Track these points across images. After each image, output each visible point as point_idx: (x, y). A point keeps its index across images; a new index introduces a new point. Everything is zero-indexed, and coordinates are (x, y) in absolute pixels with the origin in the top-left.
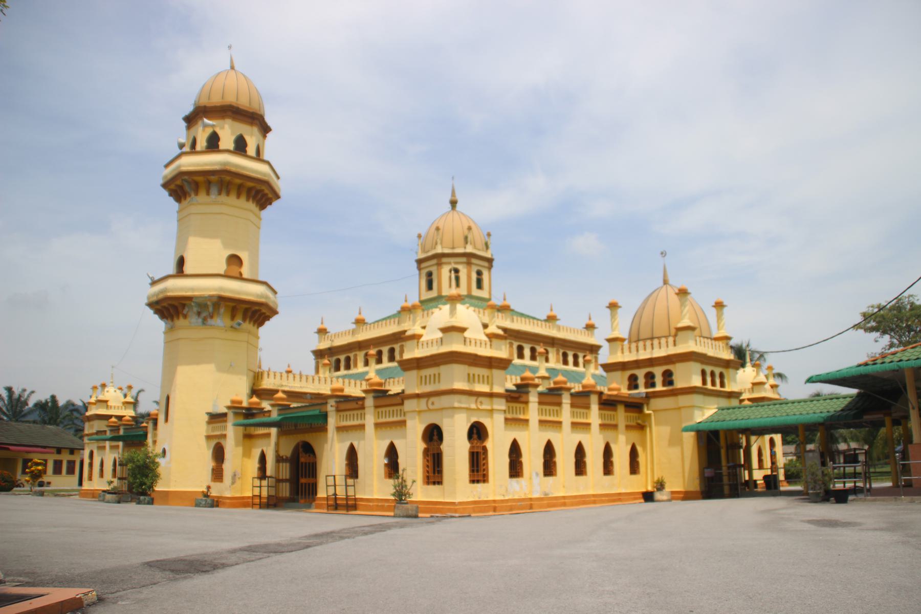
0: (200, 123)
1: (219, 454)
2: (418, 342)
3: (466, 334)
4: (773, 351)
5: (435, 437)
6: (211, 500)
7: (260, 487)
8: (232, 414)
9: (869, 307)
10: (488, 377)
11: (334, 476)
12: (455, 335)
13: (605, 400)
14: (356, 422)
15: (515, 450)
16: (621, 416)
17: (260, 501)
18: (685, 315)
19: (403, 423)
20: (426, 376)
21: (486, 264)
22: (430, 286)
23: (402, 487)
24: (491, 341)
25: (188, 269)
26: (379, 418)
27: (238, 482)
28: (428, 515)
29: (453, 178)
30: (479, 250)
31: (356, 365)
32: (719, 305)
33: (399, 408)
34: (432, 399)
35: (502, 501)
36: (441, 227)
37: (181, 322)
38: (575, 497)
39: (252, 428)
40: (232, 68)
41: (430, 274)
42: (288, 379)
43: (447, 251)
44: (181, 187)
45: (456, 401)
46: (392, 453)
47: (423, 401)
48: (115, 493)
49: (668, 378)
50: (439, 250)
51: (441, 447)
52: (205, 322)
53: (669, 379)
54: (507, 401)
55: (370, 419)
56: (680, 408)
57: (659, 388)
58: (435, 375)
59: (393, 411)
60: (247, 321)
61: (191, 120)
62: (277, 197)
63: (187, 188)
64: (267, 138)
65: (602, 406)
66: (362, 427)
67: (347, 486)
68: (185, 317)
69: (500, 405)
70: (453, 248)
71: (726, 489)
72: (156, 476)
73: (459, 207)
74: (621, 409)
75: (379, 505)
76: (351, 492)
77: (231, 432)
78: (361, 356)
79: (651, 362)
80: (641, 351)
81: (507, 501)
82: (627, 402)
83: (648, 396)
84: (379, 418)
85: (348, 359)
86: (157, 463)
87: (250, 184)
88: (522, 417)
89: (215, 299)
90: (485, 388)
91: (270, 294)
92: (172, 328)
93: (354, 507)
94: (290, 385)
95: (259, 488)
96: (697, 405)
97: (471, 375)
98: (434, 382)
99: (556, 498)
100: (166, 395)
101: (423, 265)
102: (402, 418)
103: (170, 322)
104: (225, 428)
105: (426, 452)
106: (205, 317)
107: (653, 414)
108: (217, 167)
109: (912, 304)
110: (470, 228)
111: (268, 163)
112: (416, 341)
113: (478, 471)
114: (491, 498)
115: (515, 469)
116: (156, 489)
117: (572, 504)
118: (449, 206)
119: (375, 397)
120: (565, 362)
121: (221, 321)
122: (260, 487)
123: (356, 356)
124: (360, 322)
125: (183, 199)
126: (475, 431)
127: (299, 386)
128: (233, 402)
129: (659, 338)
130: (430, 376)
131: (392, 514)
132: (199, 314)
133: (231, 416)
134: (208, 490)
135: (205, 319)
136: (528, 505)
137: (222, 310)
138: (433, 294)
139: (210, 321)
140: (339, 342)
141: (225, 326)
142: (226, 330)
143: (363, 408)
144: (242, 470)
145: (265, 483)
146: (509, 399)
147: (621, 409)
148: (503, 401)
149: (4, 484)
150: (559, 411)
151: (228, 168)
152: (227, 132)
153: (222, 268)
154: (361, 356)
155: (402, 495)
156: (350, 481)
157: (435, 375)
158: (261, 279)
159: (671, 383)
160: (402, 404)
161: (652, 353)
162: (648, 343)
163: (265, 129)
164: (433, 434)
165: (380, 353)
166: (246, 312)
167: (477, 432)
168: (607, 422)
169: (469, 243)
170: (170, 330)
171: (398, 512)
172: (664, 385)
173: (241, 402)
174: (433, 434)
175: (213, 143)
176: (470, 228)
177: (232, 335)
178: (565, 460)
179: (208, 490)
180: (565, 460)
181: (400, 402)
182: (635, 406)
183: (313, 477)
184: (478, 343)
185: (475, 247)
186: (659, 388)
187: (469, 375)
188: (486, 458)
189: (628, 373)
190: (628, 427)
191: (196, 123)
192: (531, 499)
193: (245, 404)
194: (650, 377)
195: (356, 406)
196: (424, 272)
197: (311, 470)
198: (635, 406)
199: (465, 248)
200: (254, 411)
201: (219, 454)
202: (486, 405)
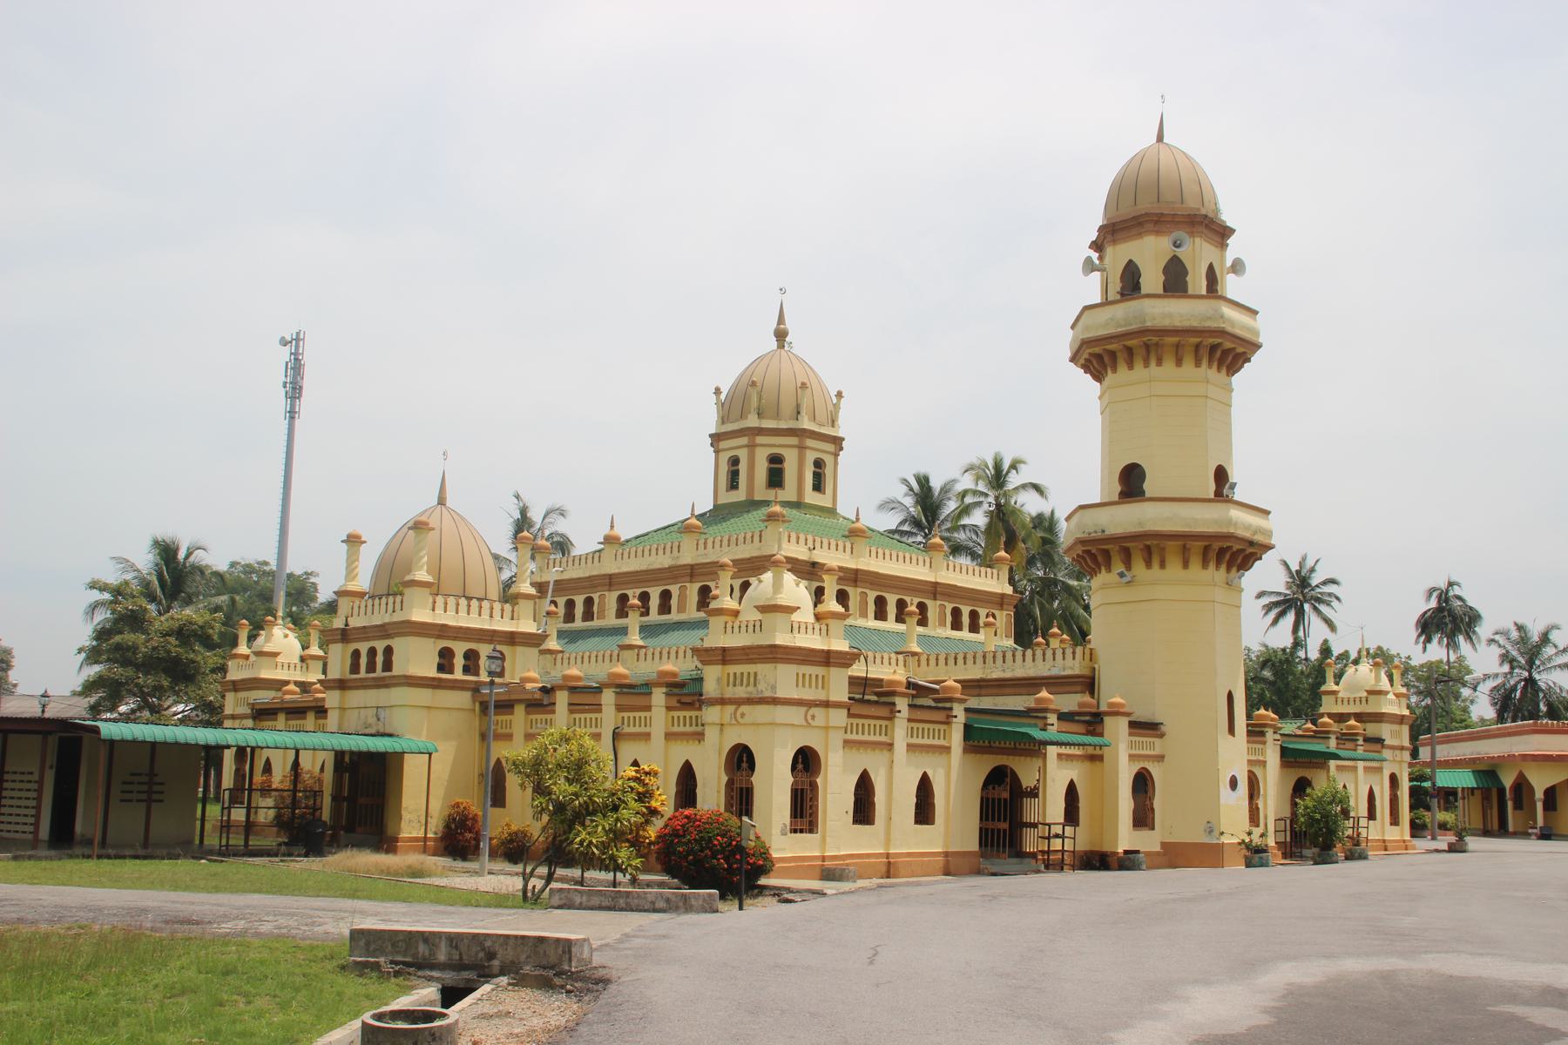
5: (745, 765)
10: (823, 677)
15: (864, 789)
19: (699, 736)
21: (830, 447)
22: (733, 484)
25: (1149, 487)
31: (602, 616)
41: (735, 461)
51: (753, 779)
53: (468, 663)
55: (900, 732)
60: (1212, 565)
61: (1110, 233)
85: (589, 602)
87: (1212, 341)
90: (820, 695)
96: (778, 721)
101: (723, 444)
104: (1263, 752)
115: (863, 810)
123: (683, 589)
129: (480, 600)
138: (740, 495)
152: (1150, 253)
167: (806, 761)
183: (987, 830)
188: (814, 798)
196: (724, 457)
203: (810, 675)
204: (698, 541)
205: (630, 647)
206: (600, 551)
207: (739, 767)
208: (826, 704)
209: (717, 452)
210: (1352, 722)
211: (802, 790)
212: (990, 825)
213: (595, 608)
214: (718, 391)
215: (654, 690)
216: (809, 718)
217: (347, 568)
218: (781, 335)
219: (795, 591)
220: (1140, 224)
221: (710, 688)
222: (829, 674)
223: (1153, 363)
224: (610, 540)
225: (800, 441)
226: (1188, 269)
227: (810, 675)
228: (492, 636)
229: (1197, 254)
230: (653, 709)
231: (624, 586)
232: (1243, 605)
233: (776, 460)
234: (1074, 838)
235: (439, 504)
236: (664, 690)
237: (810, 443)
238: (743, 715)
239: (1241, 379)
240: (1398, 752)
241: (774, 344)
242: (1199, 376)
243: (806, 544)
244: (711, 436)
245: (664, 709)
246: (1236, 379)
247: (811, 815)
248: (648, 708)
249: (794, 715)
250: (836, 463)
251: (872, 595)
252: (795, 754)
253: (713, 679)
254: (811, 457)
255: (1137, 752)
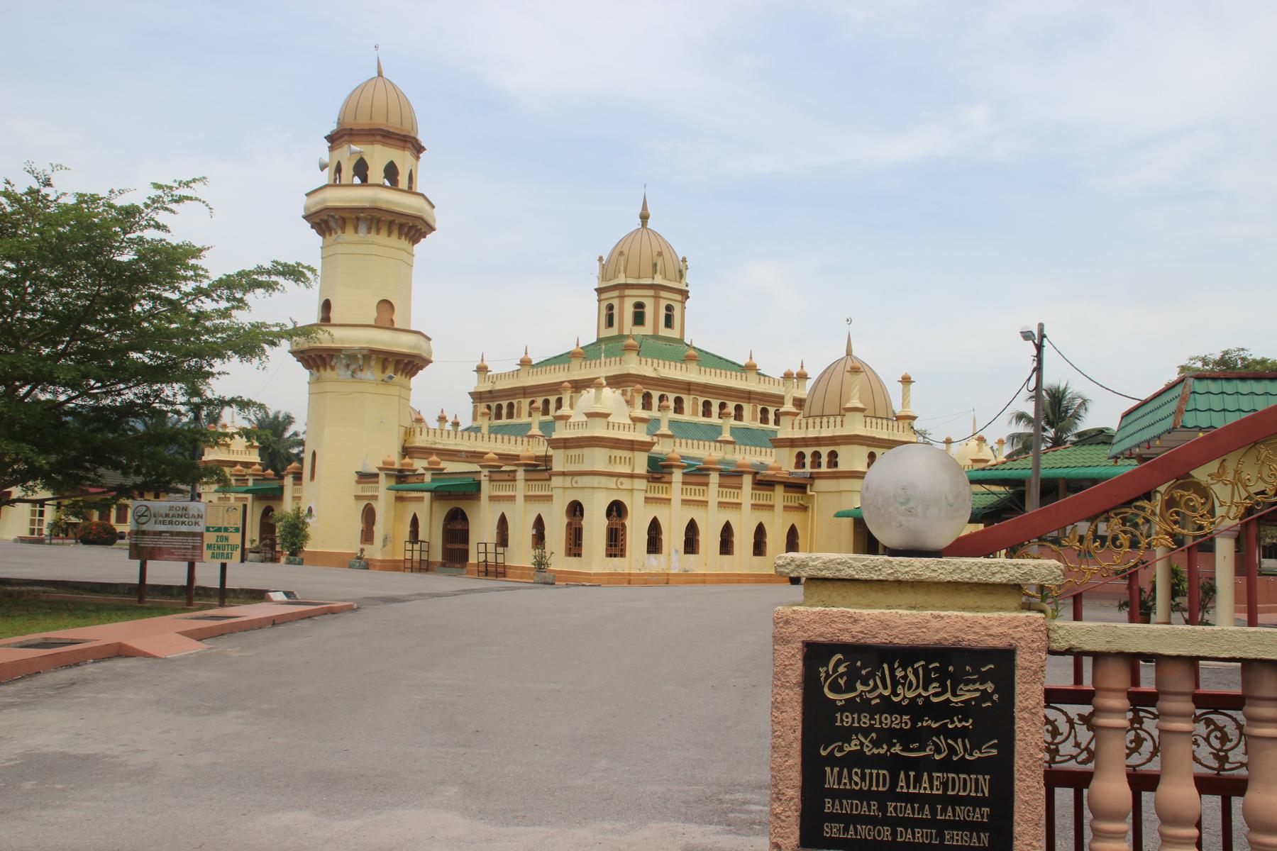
0: (346, 147)
1: (369, 516)
2: (566, 423)
3: (610, 419)
4: (1128, 396)
5: (578, 513)
6: (365, 562)
7: (412, 551)
8: (384, 476)
9: (1191, 359)
10: (630, 458)
11: (486, 544)
12: (598, 420)
13: (759, 480)
14: (508, 493)
15: (655, 527)
16: (779, 496)
17: (412, 566)
18: (855, 395)
19: (549, 498)
20: (572, 456)
21: (679, 297)
22: (610, 323)
23: (542, 558)
24: (635, 425)
25: (335, 317)
26: (529, 490)
27: (389, 545)
28: (564, 584)
29: (645, 186)
30: (670, 280)
31: (519, 416)
32: (906, 381)
33: (547, 483)
34: (576, 478)
35: (638, 575)
36: (626, 253)
37: (328, 374)
38: (718, 575)
39: (405, 492)
40: (380, 74)
41: (610, 307)
42: (442, 437)
43: (630, 281)
44: (326, 222)
45: (595, 481)
46: (539, 524)
47: (569, 479)
48: (258, 552)
49: (833, 461)
50: (622, 280)
51: (582, 522)
52: (355, 375)
54: (648, 481)
56: (841, 492)
57: (824, 468)
58: (579, 455)
59: (542, 485)
61: (334, 139)
62: (432, 229)
63: (332, 224)
64: (420, 160)
65: (756, 486)
66: (512, 498)
67: (496, 553)
68: (333, 368)
69: (642, 484)
70: (639, 278)
71: (449, 546)
72: (306, 537)
73: (650, 224)
74: (779, 490)
75: (522, 572)
76: (500, 560)
77: (383, 493)
78: (525, 403)
79: (818, 441)
80: (810, 429)
81: (643, 575)
82: (786, 482)
83: (812, 477)
84: (529, 490)
85: (511, 406)
86: (308, 523)
87: (403, 221)
88: (664, 496)
89: (366, 352)
90: (627, 470)
91: (422, 341)
92: (318, 379)
93: (504, 574)
94: (445, 442)
95: (411, 552)
97: (613, 458)
98: (571, 463)
99: (696, 575)
100: (312, 452)
101: (604, 296)
102: (550, 493)
103: (315, 371)
105: (569, 525)
106: (355, 369)
107: (816, 496)
108: (367, 205)
109: (1243, 359)
110: (660, 254)
111: (422, 195)
112: (564, 422)
113: (615, 546)
114: (627, 571)
115: (654, 544)
116: (305, 549)
117: (712, 582)
118: (639, 221)
119: (525, 471)
120: (764, 420)
121: (372, 374)
122: (412, 551)
124: (525, 363)
125: (327, 234)
126: (615, 509)
127: (454, 443)
128: (384, 463)
130: (575, 456)
131: (532, 581)
132: (348, 366)
133: (382, 477)
134: (362, 553)
135: (354, 372)
136: (666, 579)
137: (373, 363)
138: (613, 332)
139: (359, 374)
140: (500, 386)
141: (375, 380)
142: (377, 384)
143: (514, 480)
144: (393, 532)
145: (417, 547)
146: (650, 480)
147: (779, 490)
148: (645, 481)
149: (105, 537)
150: (706, 491)
151: (379, 205)
152: (378, 156)
153: (371, 316)
154: (525, 403)
155: (542, 564)
156: (500, 550)
157: (579, 455)
158: (412, 329)
159: (836, 465)
160: (550, 480)
161: (820, 432)
162: (818, 420)
163: (418, 149)
164: (576, 509)
165: (546, 402)
166: (398, 363)
167: (617, 510)
168: (757, 502)
169: (658, 273)
170: (314, 382)
171: (536, 579)
172: (829, 467)
173: (393, 464)
174: (576, 509)
175: (361, 169)
176: (660, 254)
177: (383, 389)
178: (709, 539)
179: (362, 553)
180: (709, 539)
181: (548, 478)
182: (797, 487)
184: (622, 426)
185: (665, 278)
186: (824, 468)
187: (610, 457)
188: (624, 535)
189: (797, 450)
190: (786, 508)
191: (340, 146)
192: (668, 574)
193: (397, 466)
194: (817, 455)
195: (509, 478)
196: (604, 304)
197: (464, 536)
198: (797, 487)
199: (653, 278)
200: (407, 473)
201: (369, 516)
202: (627, 483)
203: (620, 457)
204: (581, 363)
205: (533, 436)
206: (518, 370)
207: (575, 515)
208: (632, 476)
209: (599, 301)
210: (239, 467)
211: (616, 529)
212: (449, 546)
213: (515, 410)
214: (601, 259)
215: (674, 470)
216: (619, 484)
217: (903, 391)
218: (644, 218)
219: (610, 398)
220: (342, 137)
221: (557, 466)
222: (634, 458)
223: (373, 232)
224: (525, 363)
225: (655, 292)
226: (369, 164)
227: (620, 457)
228: (818, 441)
229: (403, 159)
230: (673, 484)
231: (725, 398)
232: (411, 399)
233: (639, 306)
234: (478, 553)
235: (847, 355)
236: (524, 468)
237: (663, 294)
238: (622, 484)
239: (423, 247)
240: (625, 481)
241: (637, 223)
242: (393, 243)
243: (652, 365)
244: (596, 290)
245: (681, 484)
246: (417, 248)
247: (622, 545)
248: (707, 484)
249: (611, 482)
250: (684, 308)
251: (701, 400)
252: (611, 504)
253: (560, 461)
254: (663, 304)
255: (688, 497)
